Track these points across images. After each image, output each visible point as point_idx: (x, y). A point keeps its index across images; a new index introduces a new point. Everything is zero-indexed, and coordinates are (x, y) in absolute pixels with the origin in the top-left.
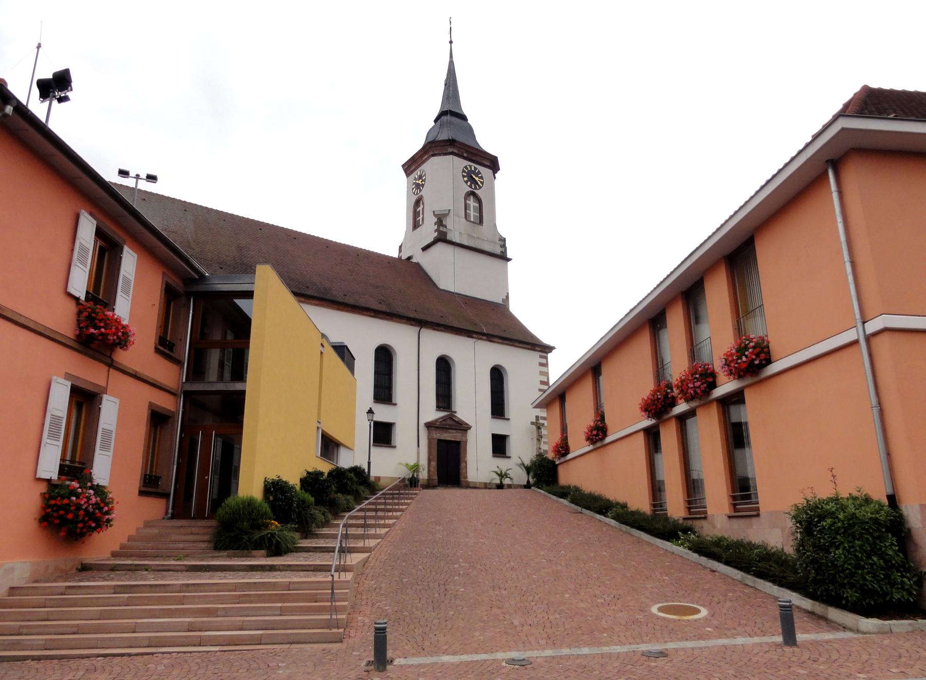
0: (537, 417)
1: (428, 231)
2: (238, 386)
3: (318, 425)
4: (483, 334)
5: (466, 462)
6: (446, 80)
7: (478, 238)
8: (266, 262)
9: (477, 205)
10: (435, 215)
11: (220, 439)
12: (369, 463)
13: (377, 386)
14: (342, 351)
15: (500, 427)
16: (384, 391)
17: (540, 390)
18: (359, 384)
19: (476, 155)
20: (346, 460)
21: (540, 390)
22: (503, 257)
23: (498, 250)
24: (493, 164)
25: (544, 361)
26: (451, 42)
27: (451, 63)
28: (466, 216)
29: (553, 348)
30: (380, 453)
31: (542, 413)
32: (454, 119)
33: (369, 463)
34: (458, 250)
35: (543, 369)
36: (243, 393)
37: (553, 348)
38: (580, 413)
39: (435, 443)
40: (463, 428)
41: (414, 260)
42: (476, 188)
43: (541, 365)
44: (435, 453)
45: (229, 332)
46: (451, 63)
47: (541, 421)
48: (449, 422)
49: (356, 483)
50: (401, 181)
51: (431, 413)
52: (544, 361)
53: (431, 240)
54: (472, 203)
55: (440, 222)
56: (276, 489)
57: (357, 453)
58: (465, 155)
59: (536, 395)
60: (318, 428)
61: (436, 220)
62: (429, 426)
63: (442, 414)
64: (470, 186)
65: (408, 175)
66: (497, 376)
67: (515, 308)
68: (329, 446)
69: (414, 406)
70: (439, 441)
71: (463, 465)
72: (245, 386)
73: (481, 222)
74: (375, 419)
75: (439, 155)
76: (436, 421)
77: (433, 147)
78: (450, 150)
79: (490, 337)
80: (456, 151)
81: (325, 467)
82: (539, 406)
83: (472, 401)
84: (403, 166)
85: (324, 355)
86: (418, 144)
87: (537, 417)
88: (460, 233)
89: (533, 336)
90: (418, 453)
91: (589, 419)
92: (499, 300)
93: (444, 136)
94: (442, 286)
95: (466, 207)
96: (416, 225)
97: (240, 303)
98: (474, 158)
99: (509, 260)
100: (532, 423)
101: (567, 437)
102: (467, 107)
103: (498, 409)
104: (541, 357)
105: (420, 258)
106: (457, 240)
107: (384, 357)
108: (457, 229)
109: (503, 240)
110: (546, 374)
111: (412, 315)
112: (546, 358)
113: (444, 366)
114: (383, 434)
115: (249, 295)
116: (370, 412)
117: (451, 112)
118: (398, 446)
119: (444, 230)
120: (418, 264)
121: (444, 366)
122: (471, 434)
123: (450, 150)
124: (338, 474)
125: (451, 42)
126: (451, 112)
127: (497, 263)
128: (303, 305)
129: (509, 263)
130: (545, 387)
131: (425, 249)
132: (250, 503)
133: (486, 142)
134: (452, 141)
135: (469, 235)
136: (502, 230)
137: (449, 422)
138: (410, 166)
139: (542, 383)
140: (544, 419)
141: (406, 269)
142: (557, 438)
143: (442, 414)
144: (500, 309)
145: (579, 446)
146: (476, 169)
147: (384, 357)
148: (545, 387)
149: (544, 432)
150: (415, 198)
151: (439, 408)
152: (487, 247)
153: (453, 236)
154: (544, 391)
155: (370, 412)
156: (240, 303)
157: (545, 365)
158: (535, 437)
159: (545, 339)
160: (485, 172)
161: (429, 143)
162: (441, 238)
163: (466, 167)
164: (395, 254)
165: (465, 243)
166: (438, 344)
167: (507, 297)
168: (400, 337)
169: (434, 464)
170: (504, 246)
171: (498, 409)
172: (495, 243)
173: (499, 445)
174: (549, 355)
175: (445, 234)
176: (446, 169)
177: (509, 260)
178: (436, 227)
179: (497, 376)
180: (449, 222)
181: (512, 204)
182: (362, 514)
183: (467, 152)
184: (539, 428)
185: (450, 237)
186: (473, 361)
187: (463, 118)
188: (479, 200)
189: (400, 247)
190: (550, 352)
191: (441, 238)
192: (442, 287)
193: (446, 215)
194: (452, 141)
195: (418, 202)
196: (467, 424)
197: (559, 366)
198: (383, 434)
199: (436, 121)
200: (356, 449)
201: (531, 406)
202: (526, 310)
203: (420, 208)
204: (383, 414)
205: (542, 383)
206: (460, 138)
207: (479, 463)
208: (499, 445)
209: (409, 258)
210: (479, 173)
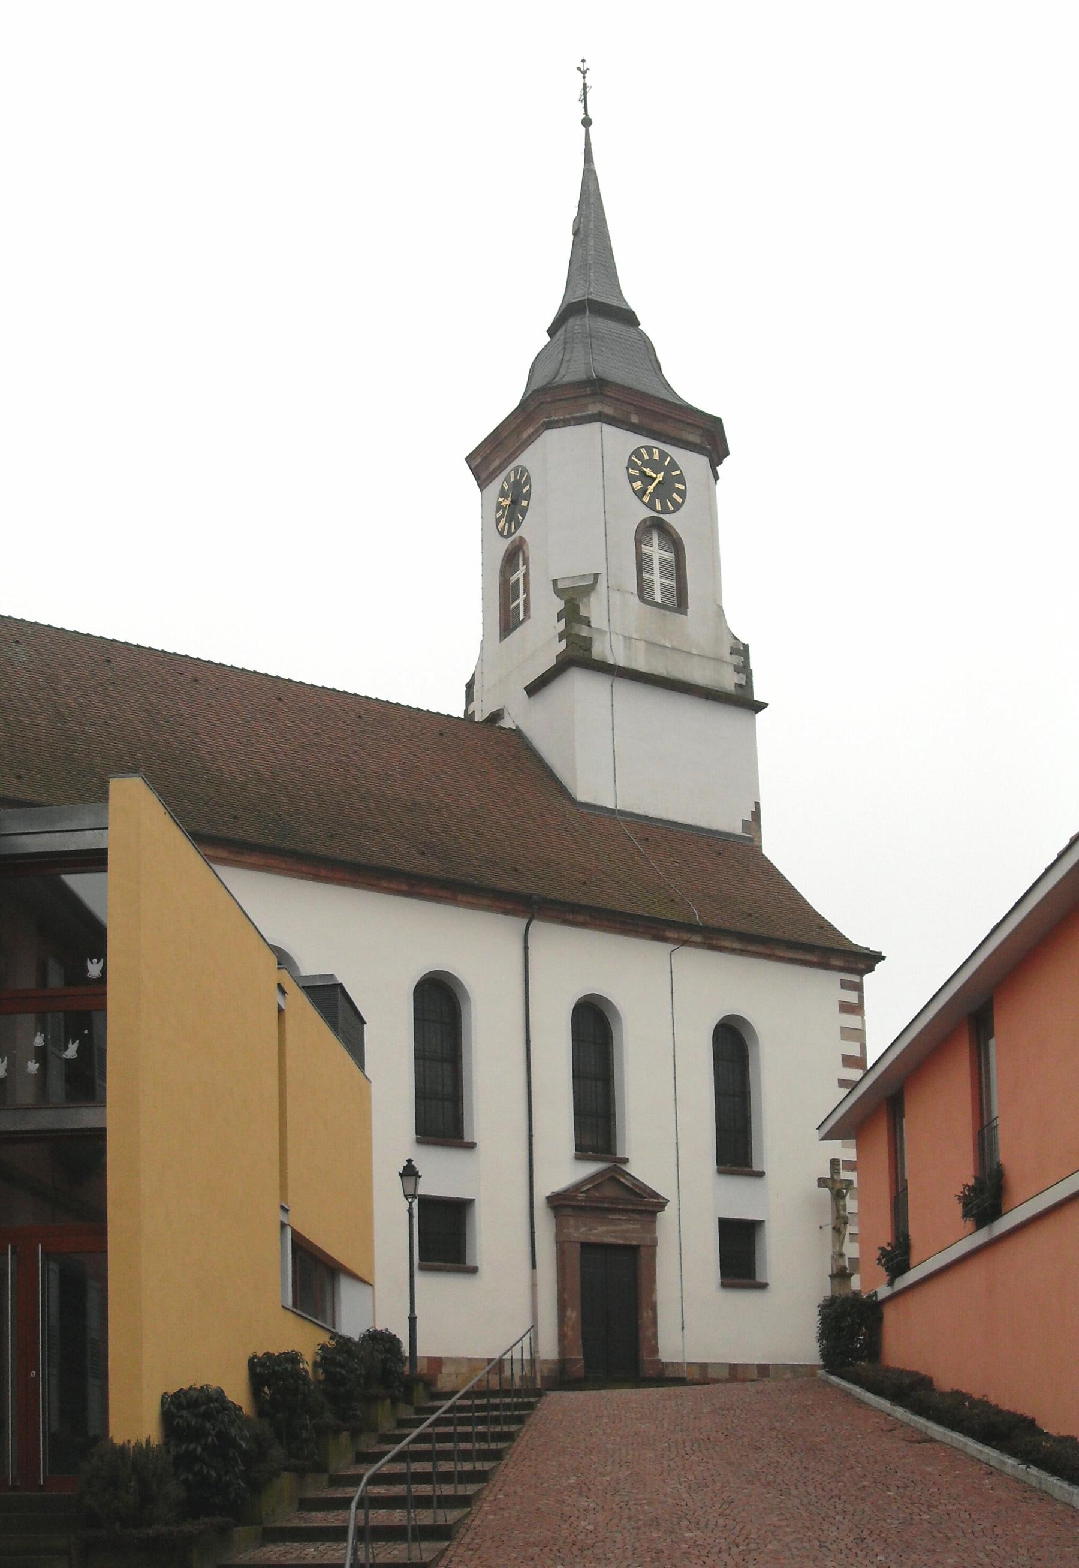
0: (834, 1163)
1: (541, 638)
2: (84, 1118)
3: (279, 998)
4: (693, 928)
5: (653, 1307)
6: (577, 222)
7: (673, 649)
8: (129, 770)
9: (669, 556)
10: (559, 592)
11: (54, 1267)
12: (412, 1320)
13: (423, 1096)
14: (332, 1001)
15: (739, 1200)
16: (442, 1117)
17: (842, 1083)
18: (377, 1092)
19: (664, 418)
20: (357, 1314)
21: (842, 1083)
22: (744, 701)
23: (729, 681)
24: (709, 438)
25: (851, 997)
26: (587, 122)
27: (589, 176)
28: (643, 589)
29: (878, 957)
30: (438, 1290)
31: (844, 1150)
32: (604, 325)
33: (412, 1320)
34: (625, 689)
35: (851, 1021)
36: (99, 1135)
37: (878, 957)
38: (941, 1161)
39: (575, 1252)
40: (646, 1204)
41: (507, 723)
42: (665, 510)
43: (847, 1008)
44: (575, 1282)
45: (52, 964)
46: (589, 176)
47: (845, 1175)
48: (610, 1191)
49: (380, 1371)
50: (467, 504)
51: (563, 1170)
52: (851, 997)
53: (548, 661)
54: (656, 551)
55: (572, 612)
56: (191, 1412)
57: (384, 1297)
58: (635, 419)
59: (828, 1098)
60: (283, 1225)
61: (559, 605)
62: (559, 1203)
63: (590, 1169)
64: (650, 506)
65: (482, 484)
66: (732, 1043)
67: (777, 848)
68: (315, 1275)
69: (516, 1156)
70: (585, 1246)
71: (646, 1314)
72: (104, 1114)
73: (679, 601)
74: (421, 1191)
75: (566, 423)
76: (577, 1188)
77: (550, 402)
78: (594, 409)
79: (711, 936)
80: (609, 410)
81: (303, 1340)
82: (834, 1133)
83: (665, 1130)
84: (469, 459)
85: (288, 1016)
86: (508, 396)
87: (834, 1163)
88: (628, 639)
89: (825, 927)
90: (534, 1286)
91: (964, 1172)
92: (731, 823)
93: (575, 372)
94: (583, 794)
95: (642, 564)
96: (508, 618)
97: (78, 883)
98: (657, 426)
99: (760, 706)
100: (822, 1182)
101: (906, 1237)
102: (634, 292)
103: (735, 1149)
104: (845, 985)
105: (521, 714)
106: (618, 657)
107: (439, 1004)
108: (620, 625)
109: (741, 651)
110: (858, 1035)
111: (503, 885)
112: (858, 988)
113: (594, 1027)
114: (443, 1234)
115: (95, 860)
116: (409, 1172)
117: (593, 308)
118: (480, 1145)
119: (584, 632)
120: (517, 732)
121: (594, 1027)
122: (666, 1218)
123: (594, 409)
124: (340, 1353)
125: (587, 122)
126: (593, 308)
127: (726, 718)
128: (227, 874)
129: (760, 716)
130: (855, 1074)
131: (534, 689)
132: (137, 1460)
133: (690, 381)
134: (600, 377)
135: (651, 644)
136: (740, 624)
137: (610, 1191)
138: (490, 459)
139: (849, 1061)
140: (850, 1166)
141: (486, 750)
142: (885, 1237)
143: (590, 1169)
144: (736, 855)
145: (943, 1236)
146: (663, 455)
147: (439, 1004)
148: (855, 1074)
149: (852, 1205)
150: (504, 545)
151: (583, 1151)
152: (699, 674)
153: (610, 648)
154: (853, 1085)
155: (409, 1172)
156: (78, 883)
157: (856, 1009)
158: (828, 1220)
159: (859, 935)
160: (690, 463)
161: (535, 391)
162: (578, 656)
163: (637, 453)
164: (457, 710)
165: (641, 664)
166: (578, 962)
167: (756, 815)
168: (476, 948)
169: (573, 1315)
170: (744, 669)
171: (735, 1149)
172: (719, 660)
173: (739, 1250)
174: (867, 978)
175: (587, 643)
176: (585, 468)
177: (760, 706)
178: (561, 626)
179: (732, 1043)
180: (595, 609)
181: (768, 554)
182: (400, 1468)
183: (640, 410)
184: (838, 1196)
185: (600, 650)
186: (669, 1002)
187: (629, 318)
188: (674, 543)
189: (470, 686)
190: (871, 969)
191: (578, 656)
192: (581, 797)
193: (588, 590)
194: (600, 377)
195: (514, 557)
196: (655, 1195)
197: (894, 1006)
198: (443, 1234)
199: (552, 331)
200: (378, 1280)
201: (817, 1135)
202: (809, 858)
203: (519, 575)
204: (443, 1175)
205: (849, 1061)
206: (618, 372)
207: (693, 1315)
208: (739, 1250)
209: (495, 717)
210: (674, 465)
